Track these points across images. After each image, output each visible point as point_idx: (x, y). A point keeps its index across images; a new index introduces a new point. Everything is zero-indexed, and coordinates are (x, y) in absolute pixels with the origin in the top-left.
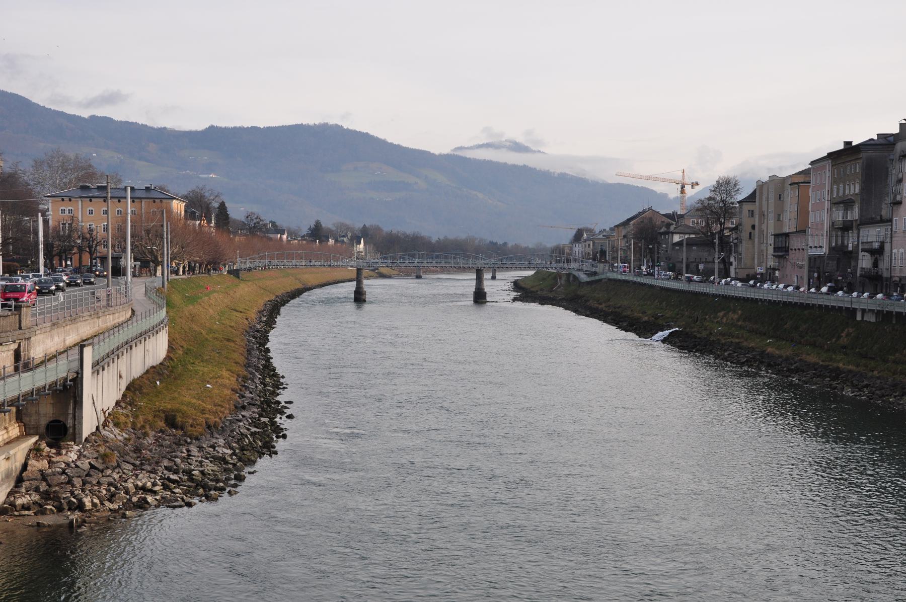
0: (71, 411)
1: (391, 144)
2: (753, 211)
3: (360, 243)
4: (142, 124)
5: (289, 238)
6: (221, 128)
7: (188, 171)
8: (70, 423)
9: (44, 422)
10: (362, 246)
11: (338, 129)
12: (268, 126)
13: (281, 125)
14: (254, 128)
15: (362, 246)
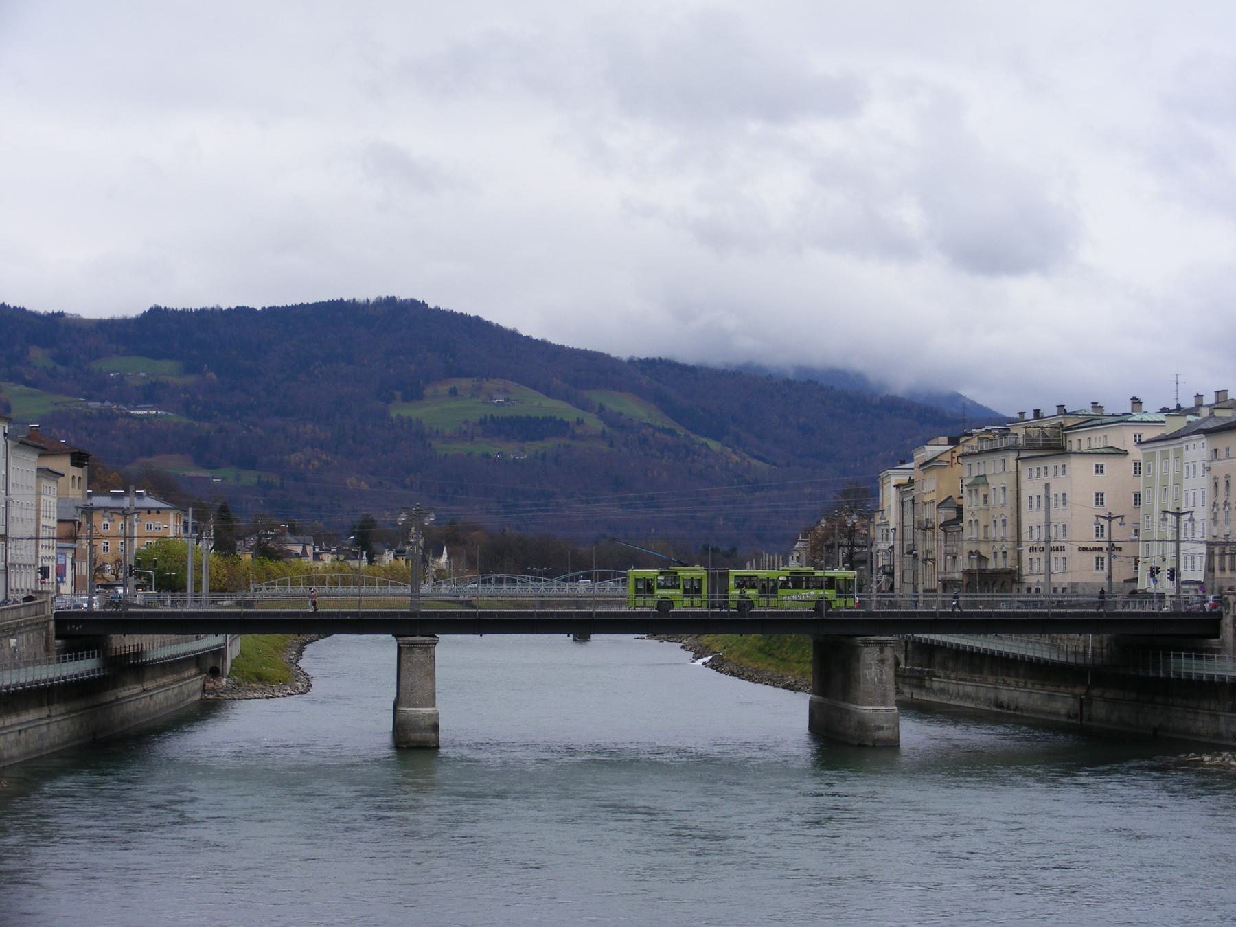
0: (221, 662)
1: (528, 338)
2: (1065, 494)
3: (441, 555)
4: (15, 307)
5: (317, 550)
6: (174, 312)
7: (107, 404)
8: (221, 669)
9: (209, 668)
10: (444, 558)
11: (414, 309)
12: (271, 305)
13: (298, 303)
14: (242, 311)
15: (444, 558)
